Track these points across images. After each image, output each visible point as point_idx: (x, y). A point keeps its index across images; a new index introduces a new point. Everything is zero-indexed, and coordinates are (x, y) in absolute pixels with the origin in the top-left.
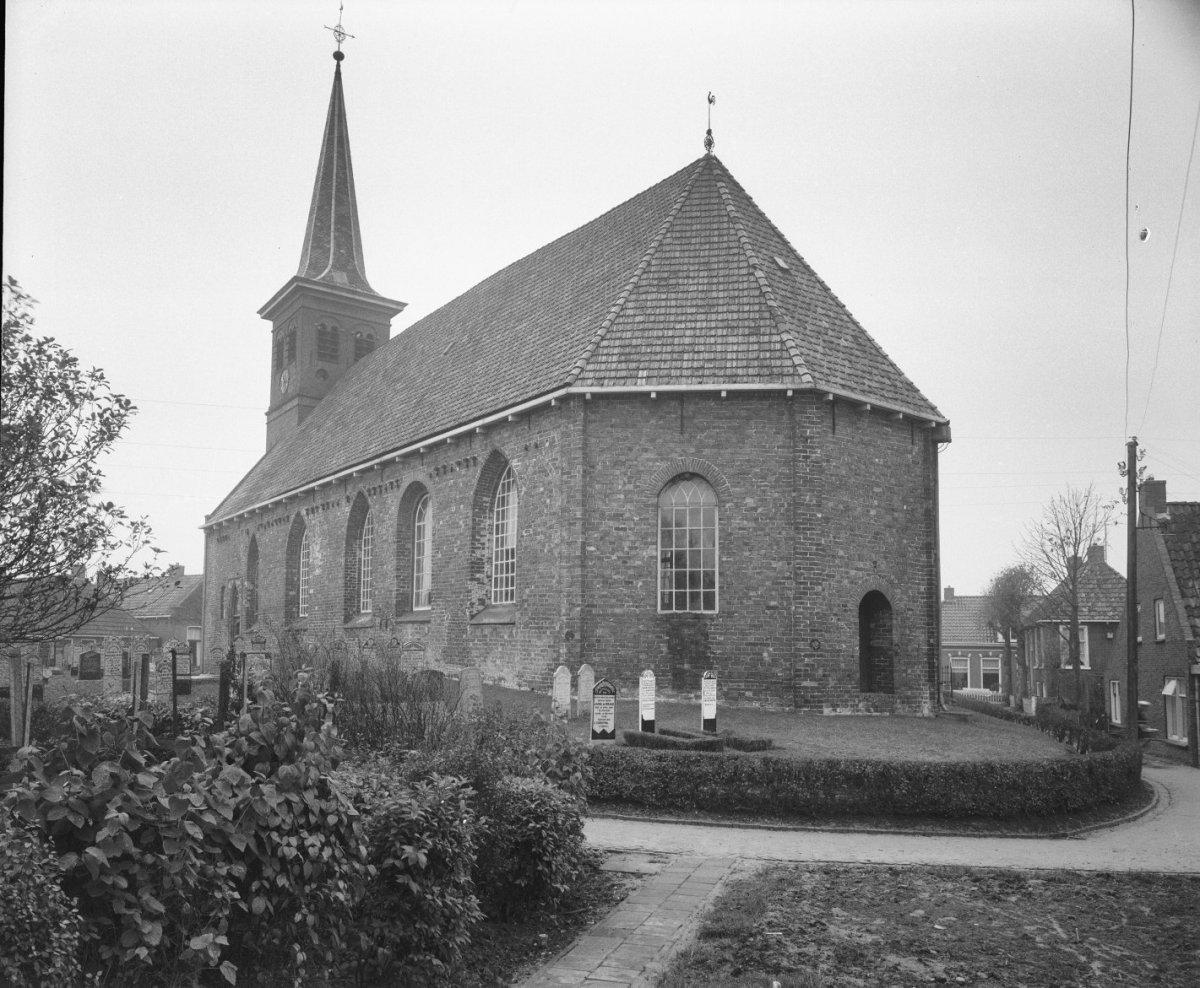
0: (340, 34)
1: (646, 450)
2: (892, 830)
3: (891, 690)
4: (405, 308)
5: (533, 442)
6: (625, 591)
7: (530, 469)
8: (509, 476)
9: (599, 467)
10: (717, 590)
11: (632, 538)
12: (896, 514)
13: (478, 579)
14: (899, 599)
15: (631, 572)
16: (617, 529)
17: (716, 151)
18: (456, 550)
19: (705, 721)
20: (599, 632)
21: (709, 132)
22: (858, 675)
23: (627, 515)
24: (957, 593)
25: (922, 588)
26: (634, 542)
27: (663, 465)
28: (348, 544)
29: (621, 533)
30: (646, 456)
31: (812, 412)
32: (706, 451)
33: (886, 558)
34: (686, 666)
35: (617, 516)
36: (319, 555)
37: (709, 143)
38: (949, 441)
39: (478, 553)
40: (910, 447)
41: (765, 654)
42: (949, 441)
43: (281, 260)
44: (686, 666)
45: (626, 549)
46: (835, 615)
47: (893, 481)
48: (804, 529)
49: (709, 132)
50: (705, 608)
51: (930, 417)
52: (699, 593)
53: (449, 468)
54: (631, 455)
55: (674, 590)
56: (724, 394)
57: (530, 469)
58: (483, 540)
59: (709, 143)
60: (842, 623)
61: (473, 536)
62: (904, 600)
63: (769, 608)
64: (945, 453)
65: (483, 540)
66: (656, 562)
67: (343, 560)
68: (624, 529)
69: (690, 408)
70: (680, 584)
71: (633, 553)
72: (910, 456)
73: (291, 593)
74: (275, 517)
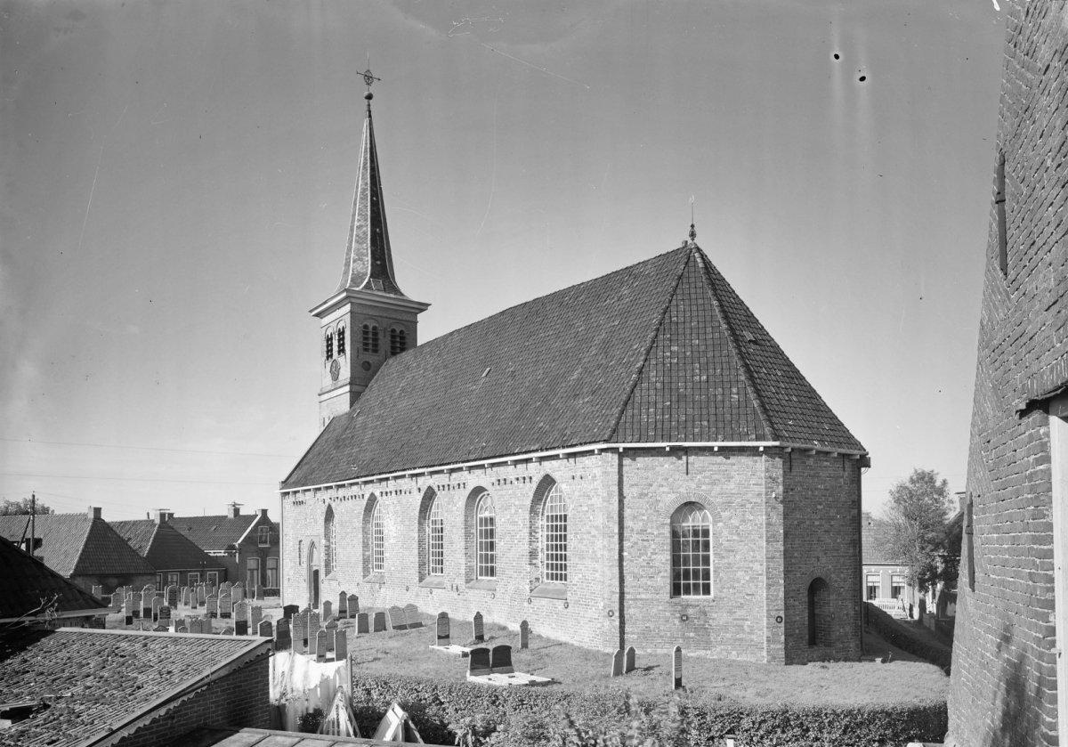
0: (369, 79)
1: (662, 486)
2: (716, 445)
3: (829, 645)
4: (429, 308)
5: (579, 474)
6: (649, 583)
7: (577, 493)
8: (556, 491)
10: (712, 582)
11: (653, 546)
12: (832, 523)
13: (535, 564)
16: (643, 540)
17: (699, 241)
18: (516, 542)
21: (692, 226)
22: (807, 636)
26: (654, 550)
27: (673, 496)
28: (420, 523)
29: (645, 543)
30: (662, 489)
33: (825, 554)
36: (393, 529)
37: (693, 235)
38: (870, 467)
39: (534, 545)
40: (842, 472)
41: (745, 627)
42: (870, 467)
45: (649, 554)
46: (792, 597)
47: (830, 499)
49: (692, 226)
50: (704, 594)
51: (856, 452)
52: (699, 584)
53: (508, 482)
54: (652, 489)
56: (716, 449)
57: (577, 493)
58: (537, 535)
59: (693, 235)
60: (797, 603)
61: (531, 534)
62: (839, 580)
63: (747, 595)
64: (866, 475)
65: (537, 535)
67: (416, 535)
68: (648, 541)
72: (842, 480)
73: (367, 553)
74: (350, 494)
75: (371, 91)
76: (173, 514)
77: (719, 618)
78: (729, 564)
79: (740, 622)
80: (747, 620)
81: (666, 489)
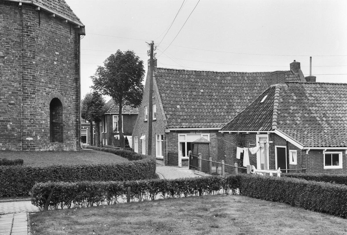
41: (8, 126)
48: (27, 68)
80: (9, 121)
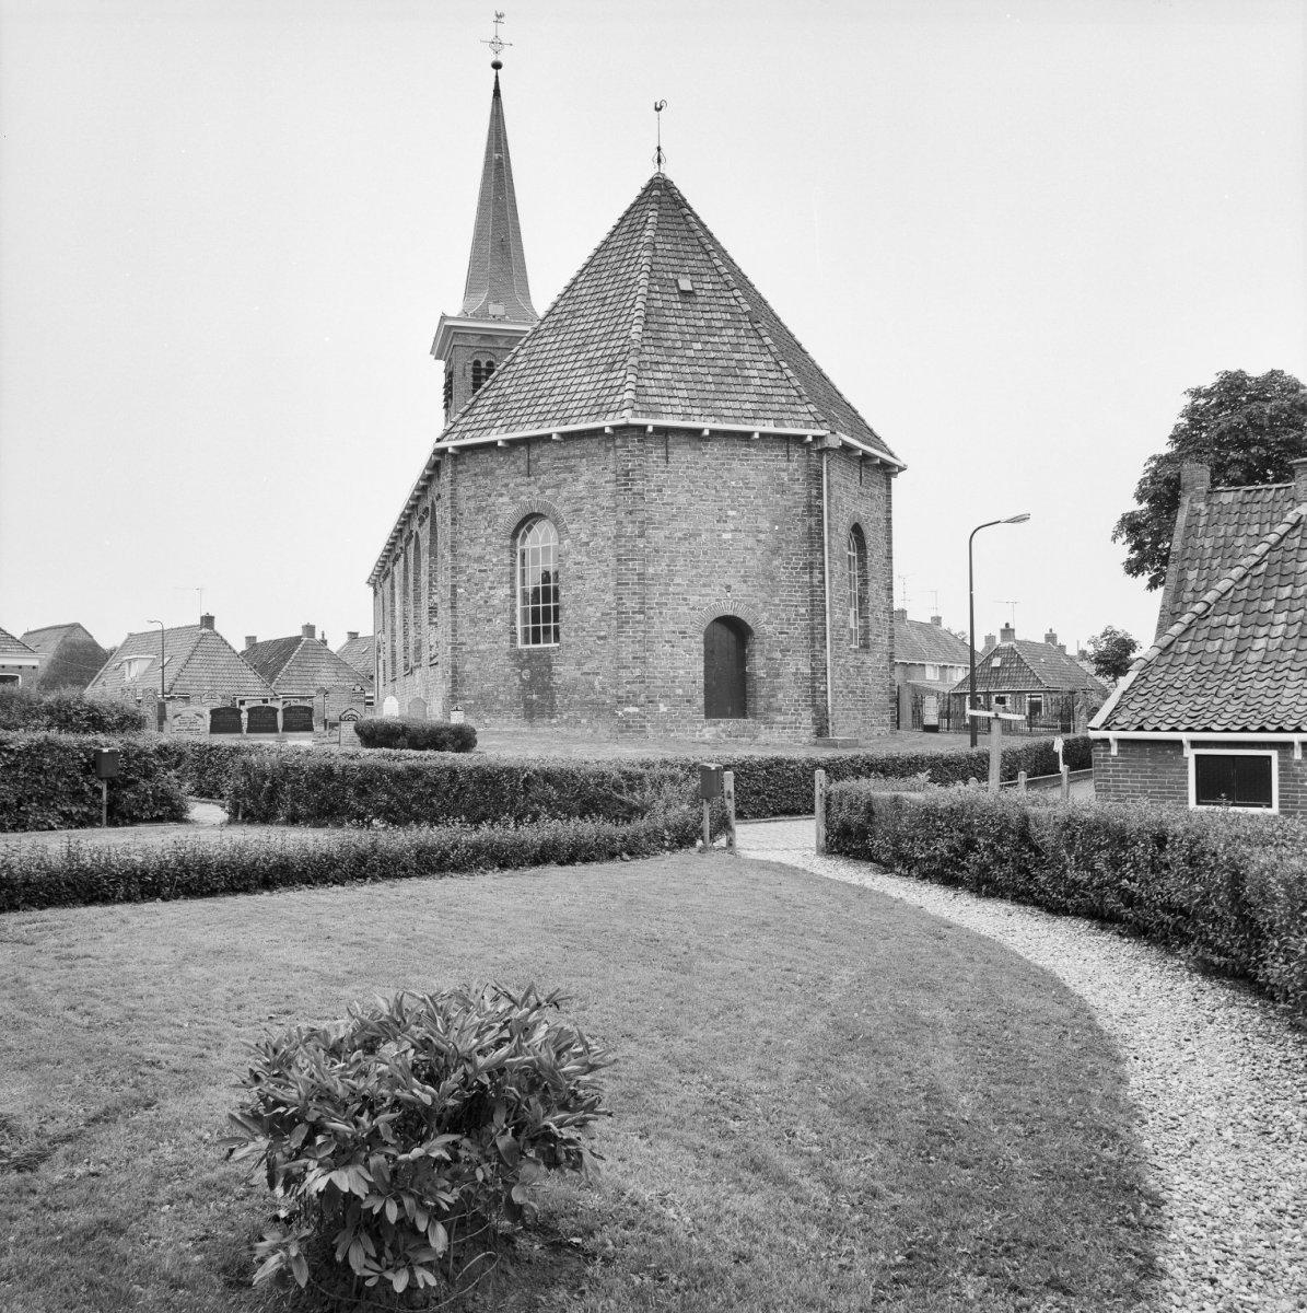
1: (501, 495)
9: (466, 514)
14: (764, 624)
15: (491, 610)
17: (670, 173)
19: (812, 811)
20: (468, 667)
23: (487, 557)
24: (945, 625)
25: (803, 610)
29: (483, 574)
30: (501, 500)
31: (633, 444)
32: (548, 492)
34: (535, 697)
35: (480, 559)
43: (445, 289)
44: (535, 697)
49: (659, 149)
54: (491, 500)
55: (530, 626)
66: (832, 635)
69: (536, 452)
70: (535, 620)
71: (492, 592)
75: (500, 59)
76: (254, 638)
77: (565, 672)
78: (577, 596)
79: (590, 678)
80: (598, 674)
81: (505, 499)
